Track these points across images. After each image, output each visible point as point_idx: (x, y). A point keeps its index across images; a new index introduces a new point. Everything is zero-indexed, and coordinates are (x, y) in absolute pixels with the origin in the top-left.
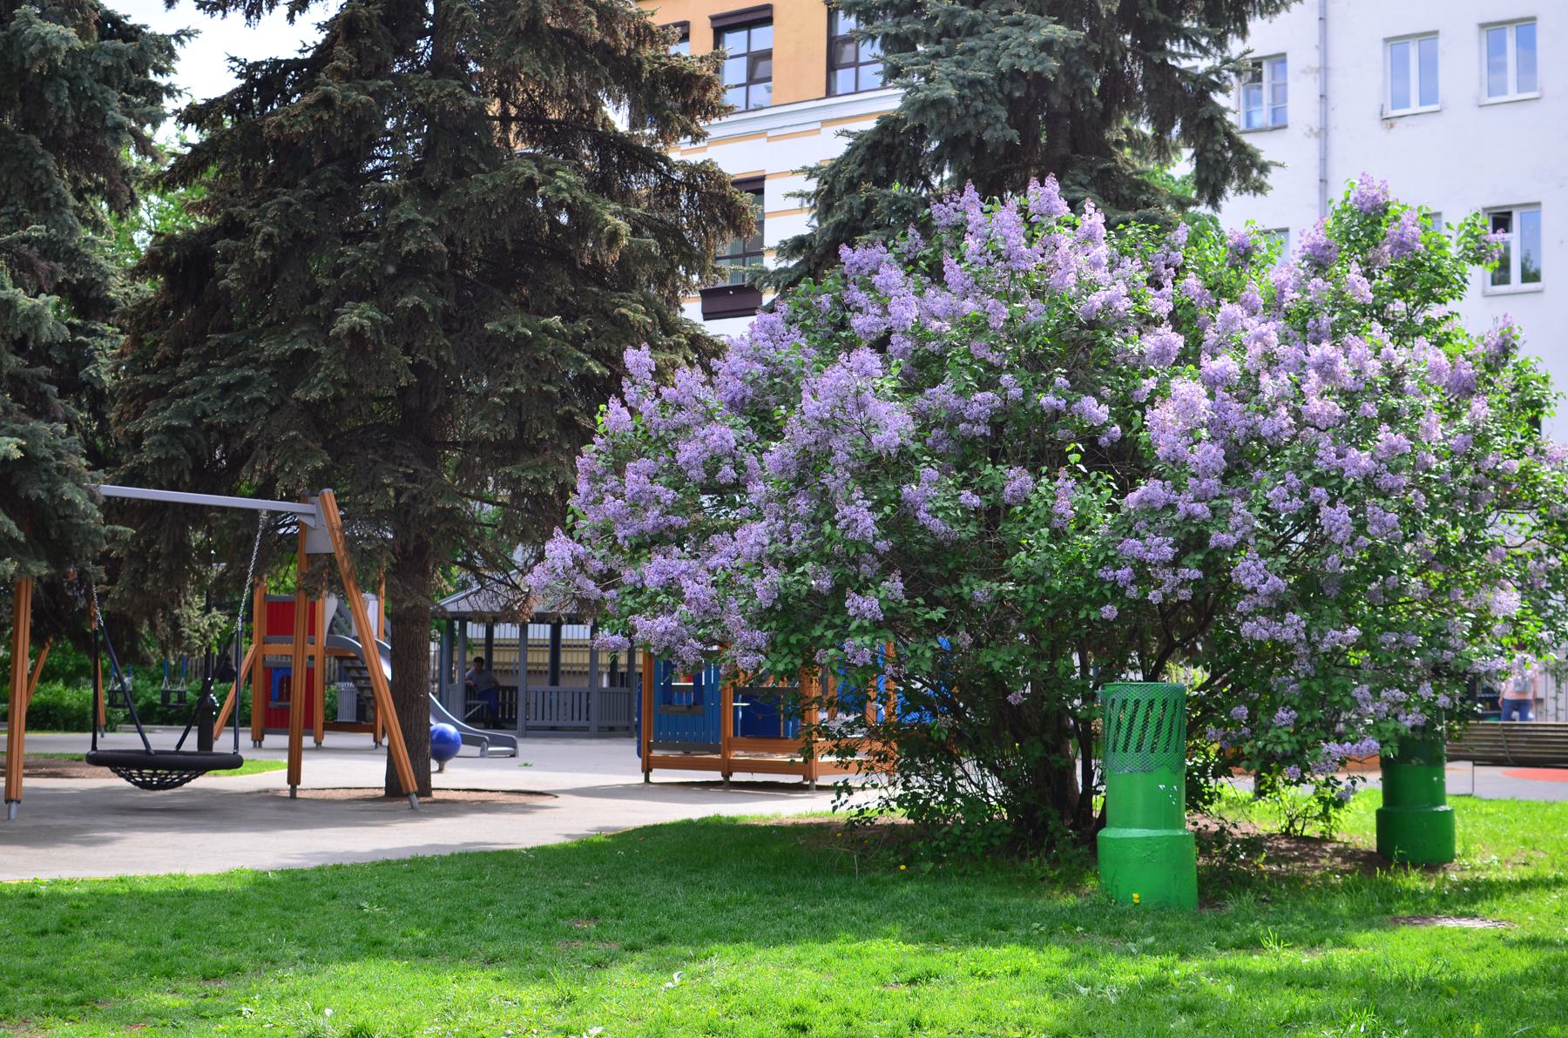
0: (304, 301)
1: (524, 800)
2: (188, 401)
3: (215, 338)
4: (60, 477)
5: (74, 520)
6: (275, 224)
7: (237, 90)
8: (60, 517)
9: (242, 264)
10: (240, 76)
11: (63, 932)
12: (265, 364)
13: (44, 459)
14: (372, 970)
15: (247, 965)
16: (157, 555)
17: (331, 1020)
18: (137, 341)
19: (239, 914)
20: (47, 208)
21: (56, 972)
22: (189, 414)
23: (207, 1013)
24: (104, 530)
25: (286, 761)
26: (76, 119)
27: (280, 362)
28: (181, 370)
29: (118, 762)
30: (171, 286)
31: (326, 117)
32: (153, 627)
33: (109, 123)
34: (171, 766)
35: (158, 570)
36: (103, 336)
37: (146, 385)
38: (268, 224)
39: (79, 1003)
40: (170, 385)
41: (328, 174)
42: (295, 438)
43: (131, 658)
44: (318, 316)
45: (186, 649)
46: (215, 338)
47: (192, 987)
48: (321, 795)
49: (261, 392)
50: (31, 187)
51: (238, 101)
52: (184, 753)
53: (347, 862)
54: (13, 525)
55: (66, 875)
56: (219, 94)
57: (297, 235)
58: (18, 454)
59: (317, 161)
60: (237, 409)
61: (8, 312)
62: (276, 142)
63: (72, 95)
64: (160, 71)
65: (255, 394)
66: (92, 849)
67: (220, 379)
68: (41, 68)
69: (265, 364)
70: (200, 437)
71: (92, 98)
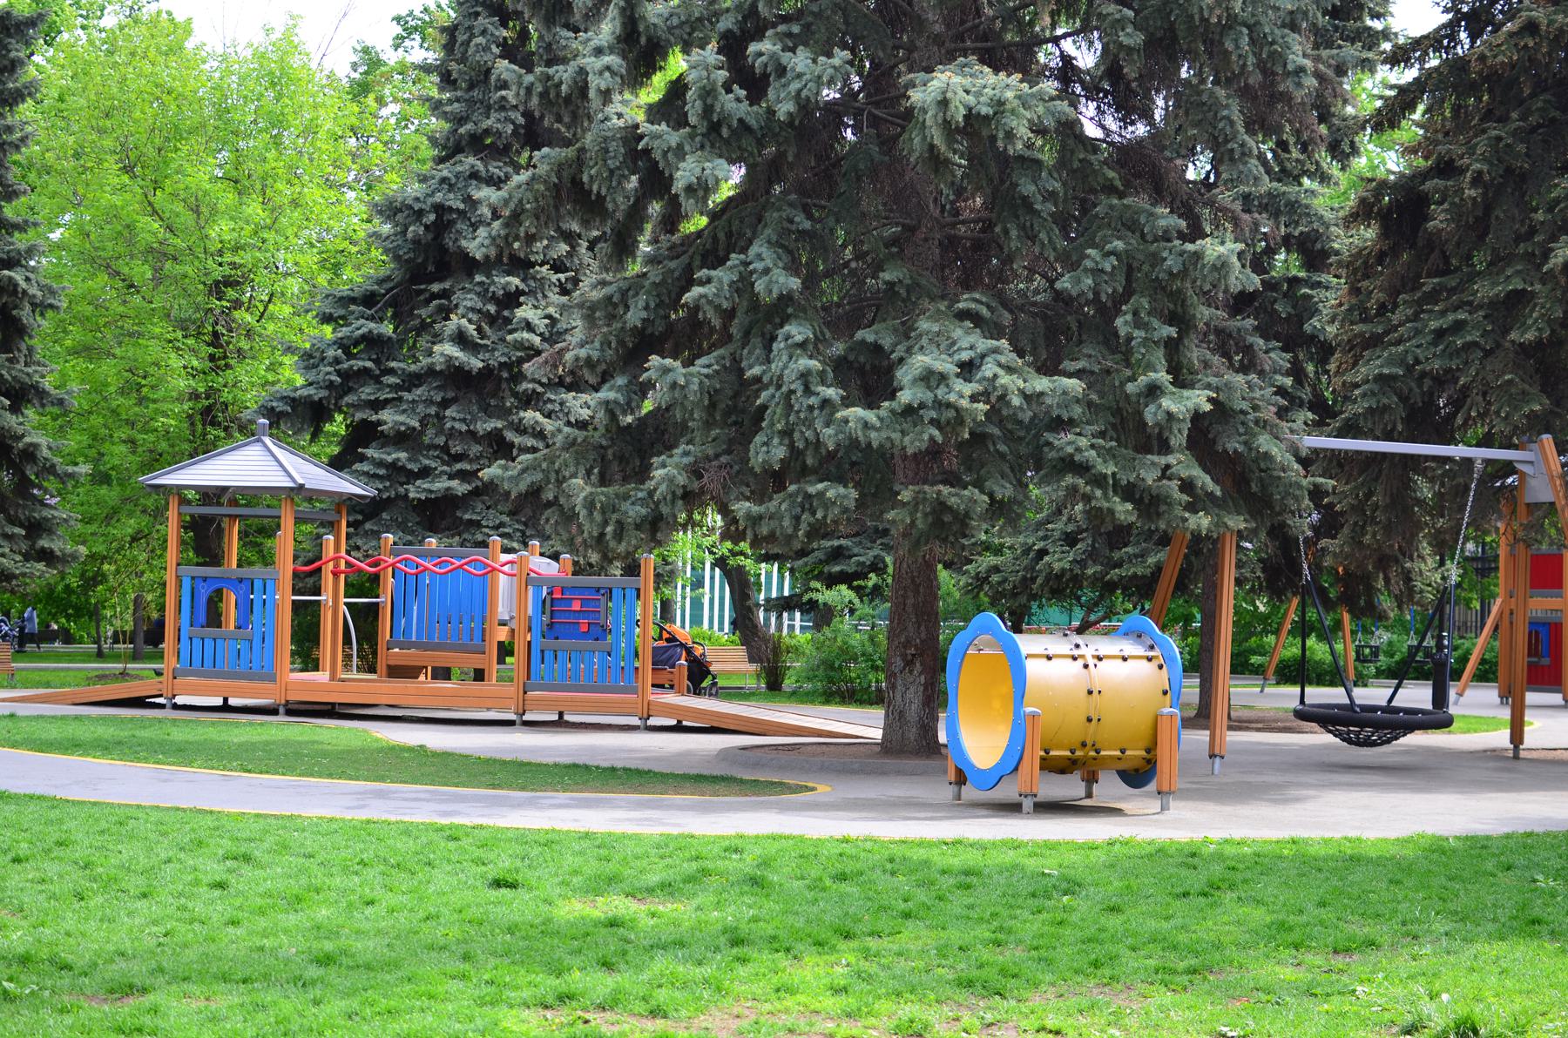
0: (1519, 239)
1: (639, 821)
2: (1401, 348)
3: (1430, 283)
4: (1257, 429)
5: (1275, 473)
6: (1485, 160)
7: (1444, 26)
8: (1262, 470)
9: (1452, 204)
10: (1446, 10)
11: (1205, 895)
12: (1480, 307)
13: (1242, 412)
14: (1518, 952)
15: (1385, 940)
16: (1376, 507)
17: (1439, 1014)
18: (1355, 291)
19: (1398, 882)
20: (1232, 159)
21: (1182, 938)
22: (1402, 361)
23: (1318, 991)
24: (1305, 482)
25: (1509, 717)
26: (1257, 66)
27: (1493, 304)
28: (1396, 318)
29: (1325, 718)
30: (1385, 233)
31: (1531, 44)
32: (1387, 580)
33: (1290, 67)
34: (1378, 726)
35: (1377, 523)
36: (1327, 288)
37: (1361, 334)
38: (1477, 161)
39: (1193, 971)
40: (1387, 333)
41: (1540, 104)
42: (1510, 382)
43: (1367, 613)
44: (1533, 254)
45: (1418, 604)
46: (1430, 283)
47: (1318, 960)
48: (1551, 755)
49: (1473, 336)
50: (1216, 138)
51: (1446, 36)
52: (1398, 710)
53: (1538, 829)
54: (1208, 479)
55: (1237, 834)
56: (1425, 32)
57: (1509, 171)
58: (1208, 407)
59: (1527, 92)
60: (1451, 355)
61: (1195, 264)
62: (1487, 79)
63: (1252, 41)
64: (1378, 16)
65: (1469, 338)
66: (1298, 806)
67: (1434, 325)
68: (1219, 17)
69: (1480, 307)
70: (1413, 385)
71: (1272, 44)
